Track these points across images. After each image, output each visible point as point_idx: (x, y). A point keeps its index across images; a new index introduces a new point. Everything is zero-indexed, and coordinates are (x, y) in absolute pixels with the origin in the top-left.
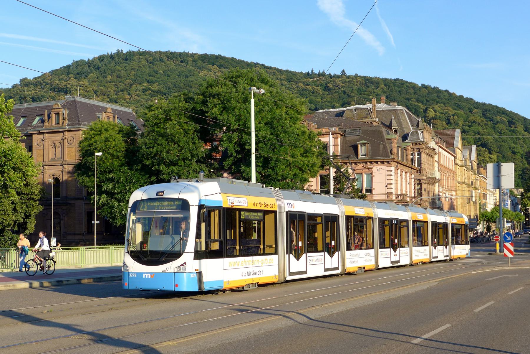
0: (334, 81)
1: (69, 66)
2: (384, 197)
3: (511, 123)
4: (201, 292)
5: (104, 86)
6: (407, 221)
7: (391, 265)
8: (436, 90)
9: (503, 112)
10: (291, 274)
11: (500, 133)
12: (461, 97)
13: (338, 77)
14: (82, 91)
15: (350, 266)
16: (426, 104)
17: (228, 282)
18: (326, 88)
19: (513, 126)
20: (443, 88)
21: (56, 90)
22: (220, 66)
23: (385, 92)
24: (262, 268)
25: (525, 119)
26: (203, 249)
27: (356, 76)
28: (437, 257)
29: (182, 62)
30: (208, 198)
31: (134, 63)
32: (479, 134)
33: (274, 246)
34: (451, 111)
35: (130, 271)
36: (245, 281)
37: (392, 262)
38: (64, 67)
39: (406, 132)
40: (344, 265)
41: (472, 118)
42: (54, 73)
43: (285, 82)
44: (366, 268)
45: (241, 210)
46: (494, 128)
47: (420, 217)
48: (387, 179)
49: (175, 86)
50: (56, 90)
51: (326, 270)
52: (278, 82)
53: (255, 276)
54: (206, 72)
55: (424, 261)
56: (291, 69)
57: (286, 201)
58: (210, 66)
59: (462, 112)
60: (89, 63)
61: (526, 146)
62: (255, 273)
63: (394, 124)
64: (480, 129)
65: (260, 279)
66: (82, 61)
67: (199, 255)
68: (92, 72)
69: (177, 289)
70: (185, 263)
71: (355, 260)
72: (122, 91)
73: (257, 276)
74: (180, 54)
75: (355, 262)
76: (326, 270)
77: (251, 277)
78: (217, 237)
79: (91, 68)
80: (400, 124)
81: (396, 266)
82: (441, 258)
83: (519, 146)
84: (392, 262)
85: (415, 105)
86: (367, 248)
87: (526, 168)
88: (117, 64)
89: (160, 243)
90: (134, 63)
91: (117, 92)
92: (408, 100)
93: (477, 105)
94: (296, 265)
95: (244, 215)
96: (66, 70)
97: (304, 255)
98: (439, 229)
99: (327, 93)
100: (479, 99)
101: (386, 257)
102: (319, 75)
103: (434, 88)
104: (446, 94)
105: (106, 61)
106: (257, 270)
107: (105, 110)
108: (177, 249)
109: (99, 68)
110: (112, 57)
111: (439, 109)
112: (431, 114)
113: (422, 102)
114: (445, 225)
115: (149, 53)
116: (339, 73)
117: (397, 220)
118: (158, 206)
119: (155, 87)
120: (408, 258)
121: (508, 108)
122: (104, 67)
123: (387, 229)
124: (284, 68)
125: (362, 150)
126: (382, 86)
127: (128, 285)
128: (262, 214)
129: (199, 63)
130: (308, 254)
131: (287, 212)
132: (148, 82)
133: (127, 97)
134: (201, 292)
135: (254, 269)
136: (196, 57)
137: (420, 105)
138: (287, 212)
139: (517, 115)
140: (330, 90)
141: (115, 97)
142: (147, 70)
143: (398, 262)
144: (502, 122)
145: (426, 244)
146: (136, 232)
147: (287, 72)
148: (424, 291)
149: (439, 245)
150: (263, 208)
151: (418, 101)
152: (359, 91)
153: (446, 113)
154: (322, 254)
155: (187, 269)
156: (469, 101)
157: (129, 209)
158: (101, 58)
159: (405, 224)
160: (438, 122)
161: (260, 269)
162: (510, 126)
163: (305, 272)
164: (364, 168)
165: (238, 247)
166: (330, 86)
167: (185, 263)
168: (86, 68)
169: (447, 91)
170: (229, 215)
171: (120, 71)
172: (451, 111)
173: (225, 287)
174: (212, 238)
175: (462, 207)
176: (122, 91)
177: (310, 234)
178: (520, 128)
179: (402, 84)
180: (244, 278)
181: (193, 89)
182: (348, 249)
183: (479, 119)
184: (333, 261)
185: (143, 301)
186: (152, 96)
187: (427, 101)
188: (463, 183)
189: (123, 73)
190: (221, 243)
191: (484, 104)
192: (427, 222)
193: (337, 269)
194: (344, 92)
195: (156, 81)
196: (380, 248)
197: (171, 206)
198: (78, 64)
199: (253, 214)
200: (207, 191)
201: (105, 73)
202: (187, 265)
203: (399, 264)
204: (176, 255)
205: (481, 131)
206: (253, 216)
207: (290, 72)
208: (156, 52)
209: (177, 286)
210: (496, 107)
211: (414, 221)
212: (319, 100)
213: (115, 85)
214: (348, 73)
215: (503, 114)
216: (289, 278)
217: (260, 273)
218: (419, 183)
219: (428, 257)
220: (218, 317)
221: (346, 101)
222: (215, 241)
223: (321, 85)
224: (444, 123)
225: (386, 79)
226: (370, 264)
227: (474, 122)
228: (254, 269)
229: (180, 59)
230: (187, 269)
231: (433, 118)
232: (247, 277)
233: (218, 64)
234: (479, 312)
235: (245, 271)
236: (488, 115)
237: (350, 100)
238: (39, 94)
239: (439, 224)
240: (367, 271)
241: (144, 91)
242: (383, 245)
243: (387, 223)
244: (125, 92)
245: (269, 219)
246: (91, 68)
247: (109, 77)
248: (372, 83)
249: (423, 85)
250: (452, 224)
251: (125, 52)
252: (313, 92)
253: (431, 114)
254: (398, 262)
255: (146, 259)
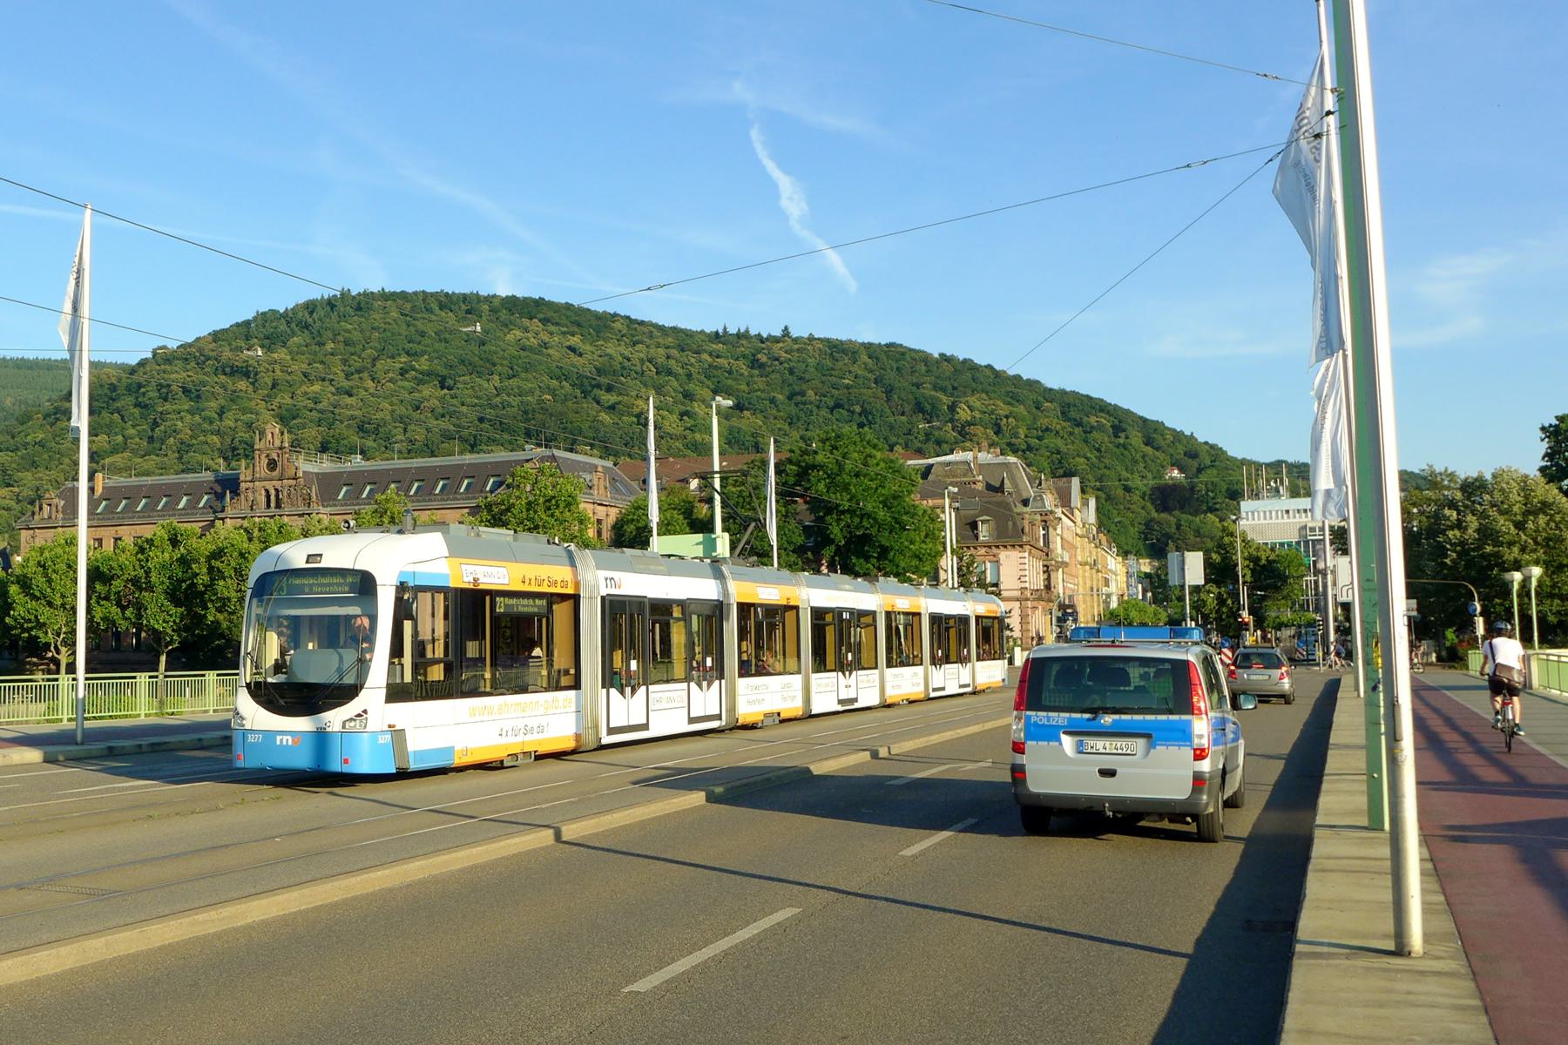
0: (769, 349)
1: (247, 323)
2: (1017, 594)
3: (1117, 430)
4: (403, 775)
5: (322, 362)
6: (873, 614)
7: (840, 708)
8: (968, 365)
9: (1101, 407)
10: (611, 731)
11: (1099, 450)
12: (1018, 377)
13: (776, 340)
14: (278, 372)
15: (893, 694)
16: (952, 395)
17: (466, 752)
18: (755, 363)
19: (1122, 435)
20: (981, 361)
21: (228, 370)
22: (545, 321)
23: (871, 371)
24: (865, 687)
25: (1145, 420)
26: (408, 678)
27: (811, 339)
28: (943, 689)
29: (468, 312)
30: (419, 568)
31: (376, 316)
32: (1058, 452)
33: (572, 671)
34: (1003, 409)
35: (248, 727)
36: (506, 747)
37: (840, 702)
38: (238, 325)
39: (1025, 496)
40: (732, 709)
41: (1043, 422)
42: (216, 336)
43: (674, 352)
44: (783, 716)
45: (494, 594)
46: (1086, 441)
47: (903, 603)
48: (1015, 569)
49: (462, 362)
50: (228, 370)
51: (692, 720)
52: (661, 351)
53: (529, 738)
54: (518, 333)
55: (912, 698)
56: (683, 325)
57: (602, 574)
58: (526, 322)
59: (1021, 409)
60: (288, 317)
61: (1150, 475)
62: (527, 730)
63: (1007, 483)
64: (1060, 443)
65: (540, 743)
66: (274, 312)
67: (396, 693)
68: (294, 334)
69: (346, 769)
70: (365, 712)
71: (760, 697)
72: (359, 371)
73: (536, 736)
74: (465, 298)
75: (761, 701)
76: (692, 720)
77: (520, 739)
78: (440, 653)
79: (293, 325)
80: (1015, 485)
81: (848, 709)
82: (952, 689)
83: (1136, 476)
84: (840, 702)
85: (932, 397)
86: (556, 686)
87: (1152, 520)
88: (343, 317)
89: (317, 665)
90: (376, 316)
91: (348, 376)
92: (918, 386)
93: (1050, 394)
94: (625, 709)
95: (502, 605)
96: (244, 332)
97: (643, 688)
98: (947, 629)
99: (757, 372)
100: (1052, 381)
101: (828, 691)
102: (739, 336)
103: (965, 361)
104: (988, 373)
105: (320, 312)
106: (533, 723)
107: (594, 468)
108: (349, 680)
109: (307, 326)
110: (331, 303)
111: (978, 404)
112: (964, 414)
113: (944, 390)
114: (963, 620)
115: (403, 295)
116: (778, 333)
117: (851, 611)
118: (311, 586)
119: (423, 364)
120: (877, 691)
121: (1111, 399)
122: (318, 324)
123: (830, 634)
124: (668, 323)
125: (984, 532)
126: (865, 358)
127: (246, 759)
128: (544, 602)
129: (504, 315)
130: (651, 688)
131: (603, 598)
132: (408, 353)
133: (370, 384)
134: (403, 775)
135: (526, 721)
136: (496, 303)
137: (940, 395)
138: (603, 598)
139: (1128, 412)
140: (762, 366)
141: (346, 384)
142: (403, 330)
143: (856, 700)
144: (1100, 428)
145: (917, 661)
146: (264, 647)
147: (674, 329)
148: (265, 924)
149: (948, 662)
150: (545, 589)
151: (935, 388)
152: (819, 367)
153: (992, 412)
154: (685, 685)
155: (379, 723)
156: (1033, 385)
157: (249, 592)
158: (310, 306)
159: (867, 620)
160: (978, 430)
161: (543, 721)
162: (1116, 436)
163: (645, 727)
164: (987, 554)
165: (488, 675)
166: (763, 358)
167: (365, 712)
168: (283, 327)
169: (989, 367)
170: (469, 607)
171: (348, 331)
172: (1003, 409)
173: (458, 761)
174: (429, 655)
175: (1085, 601)
176: (359, 371)
177: (836, 641)
178: (1136, 439)
179: (903, 354)
180: (504, 741)
181: (499, 368)
182: (889, 665)
183: (1057, 424)
184: (707, 700)
185: (268, 792)
186: (420, 382)
187: (954, 388)
188: (1086, 564)
189: (356, 336)
190: (448, 669)
191: (1063, 392)
192: (919, 614)
193: (719, 717)
194: (791, 371)
195: (424, 353)
196: (741, 675)
197: (338, 585)
198: (265, 318)
199: (525, 602)
200: (409, 557)
201: (321, 335)
202: (369, 715)
203: (856, 706)
204: (347, 693)
205: (1063, 449)
206: (525, 606)
207: (682, 331)
208: (415, 293)
209: (346, 761)
210: (1088, 397)
211: (888, 614)
212: (744, 387)
213: (345, 361)
214: (794, 333)
215: (1102, 410)
216: (607, 740)
217: (541, 729)
218: (1047, 570)
219: (922, 688)
220: (967, 723)
221: (797, 389)
222: (436, 662)
223: (744, 356)
224: (990, 432)
225: (870, 344)
226: (793, 706)
227: (1047, 429)
228: (526, 721)
229: (464, 307)
230: (379, 723)
231: (969, 424)
232: (511, 740)
233: (541, 316)
234: (915, 856)
235: (507, 725)
236: (1073, 414)
237: (804, 387)
238: (195, 377)
239: (949, 617)
240: (782, 721)
241: (403, 372)
242: (820, 664)
243: (829, 618)
244: (365, 375)
245: (561, 612)
246: (293, 325)
247: (330, 346)
248: (844, 352)
249: (942, 355)
250: (978, 618)
251: (354, 293)
252: (730, 372)
253: (964, 414)
254: (856, 700)
255: (282, 702)
